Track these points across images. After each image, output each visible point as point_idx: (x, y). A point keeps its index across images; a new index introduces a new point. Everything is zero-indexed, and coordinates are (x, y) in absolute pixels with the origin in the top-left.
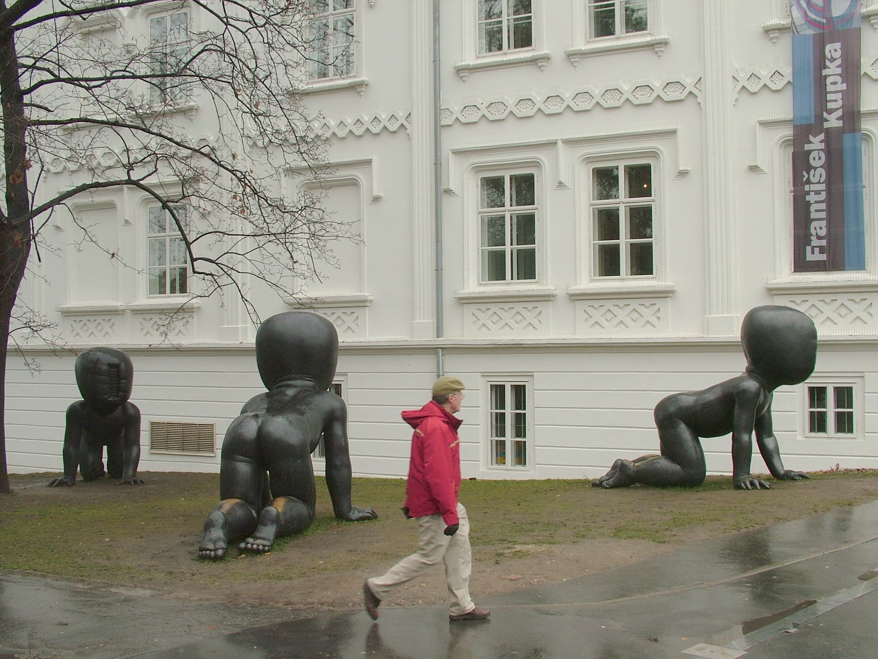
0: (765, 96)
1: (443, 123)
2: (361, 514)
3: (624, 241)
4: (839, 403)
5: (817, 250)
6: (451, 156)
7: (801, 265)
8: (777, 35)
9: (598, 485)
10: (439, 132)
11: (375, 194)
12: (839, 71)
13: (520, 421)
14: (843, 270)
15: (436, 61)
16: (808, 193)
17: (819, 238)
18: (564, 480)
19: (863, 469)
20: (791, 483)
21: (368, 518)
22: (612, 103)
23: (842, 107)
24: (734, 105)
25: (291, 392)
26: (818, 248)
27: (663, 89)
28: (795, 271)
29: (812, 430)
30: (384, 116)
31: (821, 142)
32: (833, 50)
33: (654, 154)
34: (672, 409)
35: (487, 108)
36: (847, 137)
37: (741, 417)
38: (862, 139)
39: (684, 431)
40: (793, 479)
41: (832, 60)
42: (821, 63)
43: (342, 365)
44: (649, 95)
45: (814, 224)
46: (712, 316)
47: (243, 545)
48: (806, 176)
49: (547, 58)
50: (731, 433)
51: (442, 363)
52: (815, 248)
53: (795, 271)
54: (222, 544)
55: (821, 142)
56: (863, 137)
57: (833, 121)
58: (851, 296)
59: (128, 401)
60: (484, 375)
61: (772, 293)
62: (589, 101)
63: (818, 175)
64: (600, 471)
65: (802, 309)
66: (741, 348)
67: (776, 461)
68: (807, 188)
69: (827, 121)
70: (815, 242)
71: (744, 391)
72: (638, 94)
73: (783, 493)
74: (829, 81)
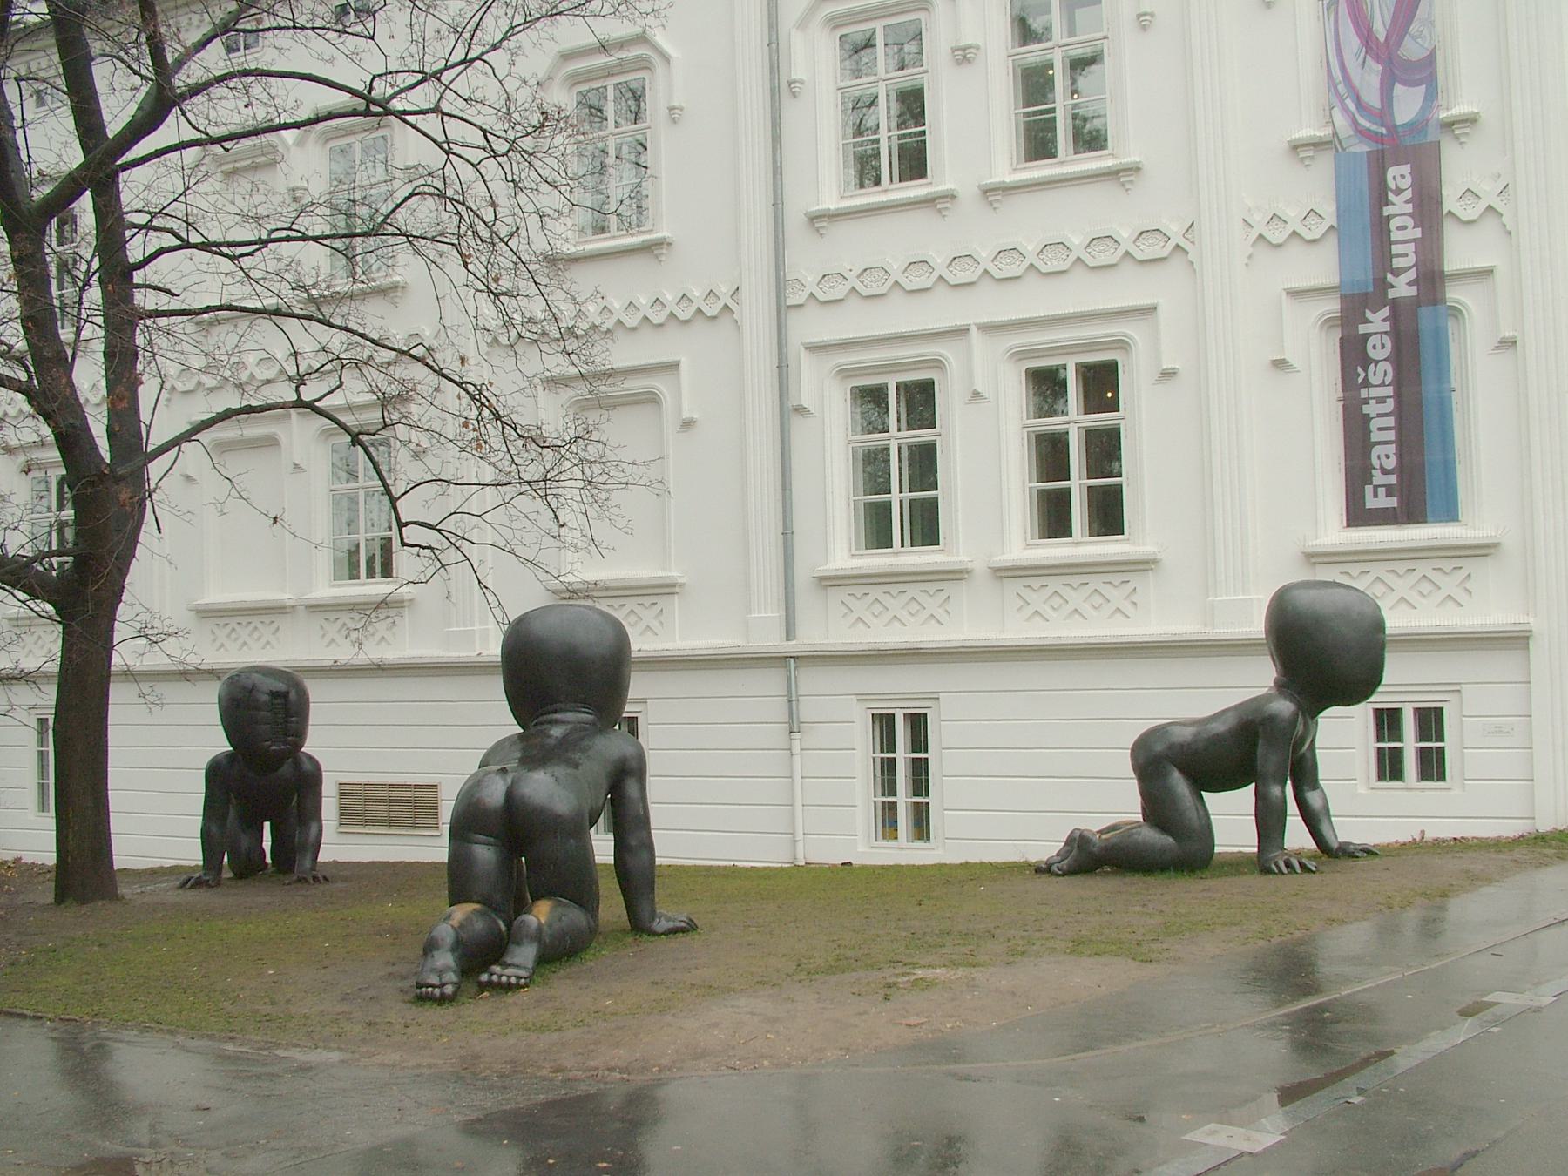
0: (1295, 248)
1: (789, 302)
2: (671, 924)
3: (1078, 484)
4: (1423, 734)
5: (1382, 491)
6: (803, 353)
7: (1357, 515)
8: (1310, 153)
9: (1043, 870)
10: (783, 316)
11: (686, 415)
12: (1409, 208)
13: (920, 770)
14: (1426, 522)
15: (777, 204)
16: (1366, 401)
17: (1385, 472)
18: (991, 864)
19: (1463, 838)
20: (1351, 863)
21: (682, 930)
22: (1055, 265)
23: (1416, 265)
24: (1247, 265)
25: (557, 732)
26: (1384, 489)
27: (1134, 242)
28: (1348, 526)
29: (1381, 777)
30: (697, 293)
31: (1384, 320)
32: (1400, 175)
33: (1122, 345)
34: (1159, 747)
35: (858, 277)
36: (1425, 312)
37: (1268, 757)
38: (1450, 315)
39: (1178, 782)
40: (1352, 856)
41: (1398, 191)
42: (1380, 195)
43: (638, 687)
44: (1112, 251)
45: (1376, 451)
46: (1220, 598)
47: (484, 977)
48: (1363, 375)
49: (951, 196)
50: (1254, 784)
51: (796, 682)
52: (1379, 489)
53: (1348, 526)
54: (451, 977)
55: (1384, 320)
56: (1449, 312)
57: (1402, 288)
58: (1066, 579)
59: (303, 750)
60: (862, 697)
61: (1313, 560)
62: (1018, 263)
63: (1381, 373)
64: (1048, 849)
65: (1361, 584)
66: (1266, 648)
67: (1325, 828)
68: (1364, 393)
69: (1393, 287)
70: (1378, 478)
71: (1272, 719)
72: (1096, 249)
73: (1336, 878)
74: (1394, 224)
